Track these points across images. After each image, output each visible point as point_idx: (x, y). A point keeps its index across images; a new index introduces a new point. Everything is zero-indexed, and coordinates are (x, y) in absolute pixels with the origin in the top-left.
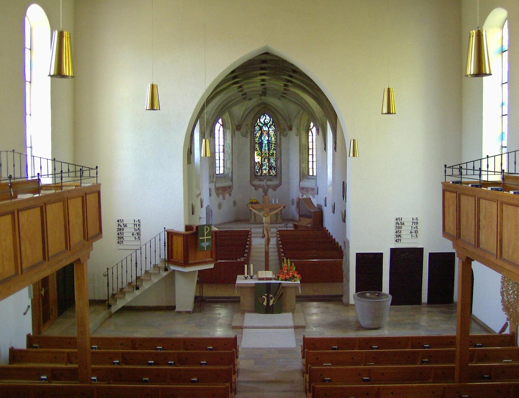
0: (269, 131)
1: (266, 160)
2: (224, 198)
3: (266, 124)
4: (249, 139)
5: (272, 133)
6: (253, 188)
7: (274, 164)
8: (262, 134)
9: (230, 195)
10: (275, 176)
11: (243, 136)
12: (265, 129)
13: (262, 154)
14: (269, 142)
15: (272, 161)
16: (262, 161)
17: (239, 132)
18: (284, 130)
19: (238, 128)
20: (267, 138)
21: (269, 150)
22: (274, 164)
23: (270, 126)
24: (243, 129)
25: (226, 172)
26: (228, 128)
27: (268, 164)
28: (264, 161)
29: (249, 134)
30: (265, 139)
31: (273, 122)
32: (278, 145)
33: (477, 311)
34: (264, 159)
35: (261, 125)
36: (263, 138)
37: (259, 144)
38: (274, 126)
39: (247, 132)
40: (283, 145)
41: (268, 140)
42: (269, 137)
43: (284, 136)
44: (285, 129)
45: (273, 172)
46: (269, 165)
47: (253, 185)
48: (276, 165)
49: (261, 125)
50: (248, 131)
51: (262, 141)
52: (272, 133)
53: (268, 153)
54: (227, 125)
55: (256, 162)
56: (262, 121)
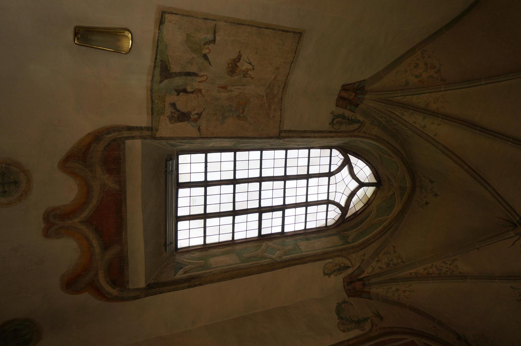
2: (56, 222)
9: (72, 283)
25: (179, 258)
50: (367, 326)
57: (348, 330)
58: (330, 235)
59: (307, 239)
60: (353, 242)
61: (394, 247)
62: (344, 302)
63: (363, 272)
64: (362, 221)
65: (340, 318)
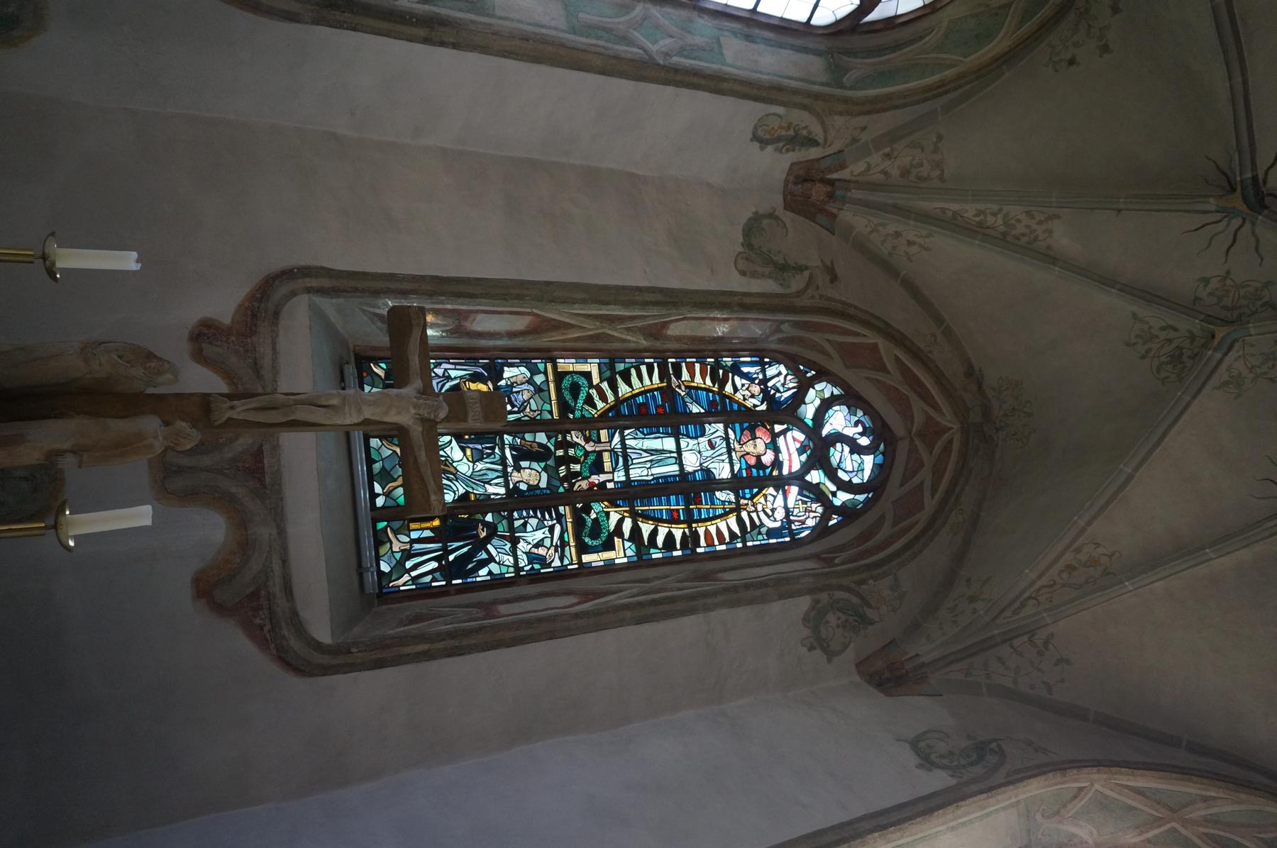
0: (781, 484)
1: (531, 475)
3: (819, 449)
4: (737, 283)
5: (774, 508)
6: (222, 305)
7: (501, 559)
8: (746, 420)
10: (384, 594)
11: (751, 229)
12: (791, 449)
13: (589, 426)
14: (693, 488)
15: (534, 535)
16: (519, 428)
17: (779, 200)
18: (858, 620)
19: (811, 192)
20: (722, 471)
21: (631, 494)
22: (501, 559)
23: (816, 492)
24: (797, 238)
26: (837, 72)
27: (497, 490)
28: (523, 454)
29: (768, 286)
30: (704, 453)
31: (843, 510)
32: (701, 581)
33: (480, 317)
34: (539, 454)
35: (808, 411)
36: (716, 429)
37: (668, 392)
38: (821, 530)
39: (782, 269)
40: (736, 626)
41: (709, 482)
42: (736, 484)
43: (814, 619)
44: (865, 621)
45: (413, 558)
46: (486, 503)
47: (263, 305)
48: (497, 582)
49: (808, 411)
50: (797, 283)
51: (699, 424)
52: (774, 508)
53: (600, 493)
54: (859, 67)
55: (508, 372)
56: (838, 420)
57: (754, 275)
58: (806, 50)
59: (748, 38)
60: (851, 88)
61: (940, 137)
62: (772, 215)
63: (842, 166)
64: (897, 47)
65: (748, 244)
